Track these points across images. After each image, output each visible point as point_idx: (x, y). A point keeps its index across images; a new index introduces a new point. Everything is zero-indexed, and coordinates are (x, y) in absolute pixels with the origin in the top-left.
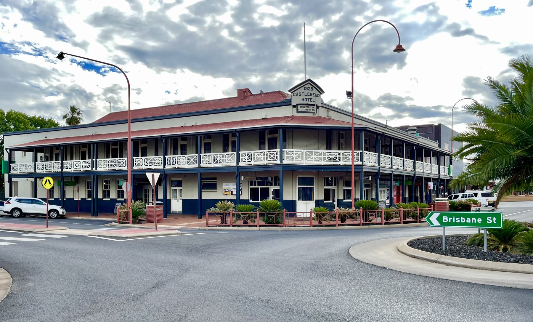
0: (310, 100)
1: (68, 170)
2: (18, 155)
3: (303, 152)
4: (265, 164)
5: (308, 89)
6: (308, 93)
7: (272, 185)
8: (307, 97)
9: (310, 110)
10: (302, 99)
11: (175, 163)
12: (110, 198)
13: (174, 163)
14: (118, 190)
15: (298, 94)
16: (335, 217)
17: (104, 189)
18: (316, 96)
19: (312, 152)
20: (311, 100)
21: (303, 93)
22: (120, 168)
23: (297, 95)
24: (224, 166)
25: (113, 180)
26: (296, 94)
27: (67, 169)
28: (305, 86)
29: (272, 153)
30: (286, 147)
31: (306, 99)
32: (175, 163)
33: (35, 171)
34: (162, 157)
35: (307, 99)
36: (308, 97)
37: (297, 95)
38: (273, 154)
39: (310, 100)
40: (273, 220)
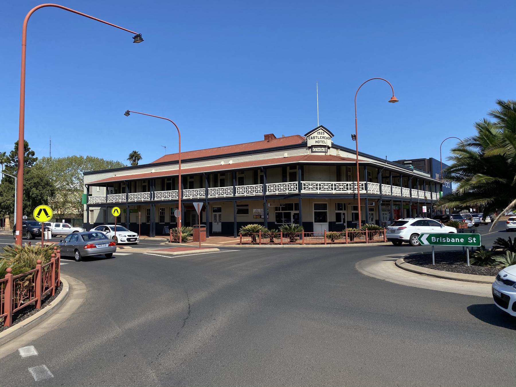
0: (322, 142)
2: (95, 190)
3: (348, 184)
4: (287, 193)
6: (321, 137)
8: (320, 140)
9: (323, 150)
10: (316, 142)
14: (171, 216)
15: (313, 138)
17: (171, 214)
19: (325, 183)
20: (323, 142)
21: (316, 137)
23: (312, 138)
24: (254, 195)
25: (167, 208)
26: (311, 138)
27: (340, 191)
28: (318, 131)
31: (319, 142)
33: (107, 202)
35: (320, 142)
36: (321, 140)
38: (293, 185)
39: (322, 142)
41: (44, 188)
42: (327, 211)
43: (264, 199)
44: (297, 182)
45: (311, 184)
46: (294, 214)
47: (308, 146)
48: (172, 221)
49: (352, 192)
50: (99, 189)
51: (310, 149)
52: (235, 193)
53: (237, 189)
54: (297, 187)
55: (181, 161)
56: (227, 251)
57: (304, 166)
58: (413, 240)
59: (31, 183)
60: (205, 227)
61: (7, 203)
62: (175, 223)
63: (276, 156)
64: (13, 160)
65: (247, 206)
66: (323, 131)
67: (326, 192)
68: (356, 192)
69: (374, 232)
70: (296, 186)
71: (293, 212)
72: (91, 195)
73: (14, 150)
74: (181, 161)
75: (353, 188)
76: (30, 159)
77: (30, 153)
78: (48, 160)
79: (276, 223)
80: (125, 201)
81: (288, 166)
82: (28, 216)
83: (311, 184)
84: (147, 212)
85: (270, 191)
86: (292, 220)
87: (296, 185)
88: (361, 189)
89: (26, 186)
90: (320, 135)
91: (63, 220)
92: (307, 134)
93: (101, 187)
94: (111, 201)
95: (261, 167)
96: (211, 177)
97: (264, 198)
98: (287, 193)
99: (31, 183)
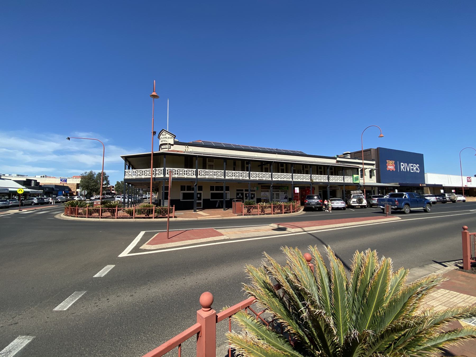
1: (254, 178)
5: (164, 135)
8: (163, 140)
11: (278, 178)
13: (284, 178)
16: (155, 211)
18: (168, 138)
22: (281, 179)
27: (202, 176)
30: (263, 171)
32: (278, 178)
36: (163, 139)
38: (212, 172)
40: (162, 211)
45: (181, 170)
56: (457, 213)
60: (241, 201)
67: (181, 176)
68: (167, 176)
69: (107, 209)
70: (270, 175)
75: (155, 173)
81: (280, 163)
88: (174, 174)
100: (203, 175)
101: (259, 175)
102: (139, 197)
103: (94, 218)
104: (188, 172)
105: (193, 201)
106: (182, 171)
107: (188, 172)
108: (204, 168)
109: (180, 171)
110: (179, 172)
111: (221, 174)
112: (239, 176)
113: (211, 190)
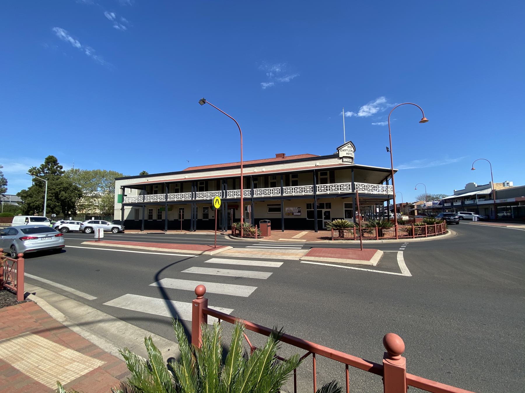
2: (127, 191)
4: (339, 193)
5: (350, 147)
7: (324, 209)
8: (349, 152)
12: (153, 219)
15: (344, 150)
17: (203, 212)
23: (343, 151)
24: (303, 195)
25: (200, 207)
26: (342, 150)
27: (307, 193)
28: (348, 145)
29: (267, 190)
33: (144, 201)
34: (143, 196)
37: (343, 151)
41: (72, 192)
42: (344, 209)
43: (252, 201)
44: (221, 191)
45: (361, 185)
46: (325, 211)
47: (340, 157)
48: (158, 219)
49: (386, 193)
50: (131, 192)
51: (341, 160)
52: (144, 200)
53: (229, 192)
54: (280, 191)
55: (243, 165)
57: (336, 171)
58: (89, 229)
59: (61, 187)
61: (36, 203)
62: (161, 220)
63: (308, 164)
64: (43, 172)
65: (280, 205)
66: (351, 146)
70: (279, 190)
71: (324, 211)
72: (126, 196)
73: (44, 164)
74: (243, 165)
76: (59, 171)
77: (59, 167)
78: (77, 171)
79: (307, 219)
80: (165, 200)
81: (270, 175)
82: (57, 214)
83: (298, 188)
84: (157, 211)
85: (230, 195)
86: (323, 217)
87: (279, 190)
89: (55, 190)
90: (349, 149)
91: (93, 218)
92: (338, 150)
93: (132, 189)
94: (148, 200)
95: (250, 176)
96: (284, 176)
97: (252, 200)
98: (339, 193)
99: (61, 187)
100: (323, 191)
101: (189, 196)
102: (500, 215)
103: (386, 239)
104: (342, 187)
105: (318, 219)
106: (334, 186)
107: (358, 186)
108: (287, 185)
109: (344, 186)
110: (331, 187)
111: (286, 191)
112: (234, 195)
113: (307, 209)
